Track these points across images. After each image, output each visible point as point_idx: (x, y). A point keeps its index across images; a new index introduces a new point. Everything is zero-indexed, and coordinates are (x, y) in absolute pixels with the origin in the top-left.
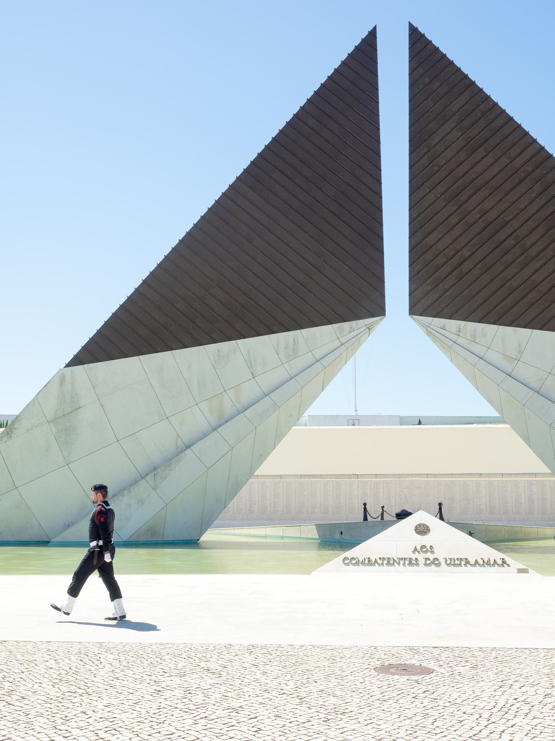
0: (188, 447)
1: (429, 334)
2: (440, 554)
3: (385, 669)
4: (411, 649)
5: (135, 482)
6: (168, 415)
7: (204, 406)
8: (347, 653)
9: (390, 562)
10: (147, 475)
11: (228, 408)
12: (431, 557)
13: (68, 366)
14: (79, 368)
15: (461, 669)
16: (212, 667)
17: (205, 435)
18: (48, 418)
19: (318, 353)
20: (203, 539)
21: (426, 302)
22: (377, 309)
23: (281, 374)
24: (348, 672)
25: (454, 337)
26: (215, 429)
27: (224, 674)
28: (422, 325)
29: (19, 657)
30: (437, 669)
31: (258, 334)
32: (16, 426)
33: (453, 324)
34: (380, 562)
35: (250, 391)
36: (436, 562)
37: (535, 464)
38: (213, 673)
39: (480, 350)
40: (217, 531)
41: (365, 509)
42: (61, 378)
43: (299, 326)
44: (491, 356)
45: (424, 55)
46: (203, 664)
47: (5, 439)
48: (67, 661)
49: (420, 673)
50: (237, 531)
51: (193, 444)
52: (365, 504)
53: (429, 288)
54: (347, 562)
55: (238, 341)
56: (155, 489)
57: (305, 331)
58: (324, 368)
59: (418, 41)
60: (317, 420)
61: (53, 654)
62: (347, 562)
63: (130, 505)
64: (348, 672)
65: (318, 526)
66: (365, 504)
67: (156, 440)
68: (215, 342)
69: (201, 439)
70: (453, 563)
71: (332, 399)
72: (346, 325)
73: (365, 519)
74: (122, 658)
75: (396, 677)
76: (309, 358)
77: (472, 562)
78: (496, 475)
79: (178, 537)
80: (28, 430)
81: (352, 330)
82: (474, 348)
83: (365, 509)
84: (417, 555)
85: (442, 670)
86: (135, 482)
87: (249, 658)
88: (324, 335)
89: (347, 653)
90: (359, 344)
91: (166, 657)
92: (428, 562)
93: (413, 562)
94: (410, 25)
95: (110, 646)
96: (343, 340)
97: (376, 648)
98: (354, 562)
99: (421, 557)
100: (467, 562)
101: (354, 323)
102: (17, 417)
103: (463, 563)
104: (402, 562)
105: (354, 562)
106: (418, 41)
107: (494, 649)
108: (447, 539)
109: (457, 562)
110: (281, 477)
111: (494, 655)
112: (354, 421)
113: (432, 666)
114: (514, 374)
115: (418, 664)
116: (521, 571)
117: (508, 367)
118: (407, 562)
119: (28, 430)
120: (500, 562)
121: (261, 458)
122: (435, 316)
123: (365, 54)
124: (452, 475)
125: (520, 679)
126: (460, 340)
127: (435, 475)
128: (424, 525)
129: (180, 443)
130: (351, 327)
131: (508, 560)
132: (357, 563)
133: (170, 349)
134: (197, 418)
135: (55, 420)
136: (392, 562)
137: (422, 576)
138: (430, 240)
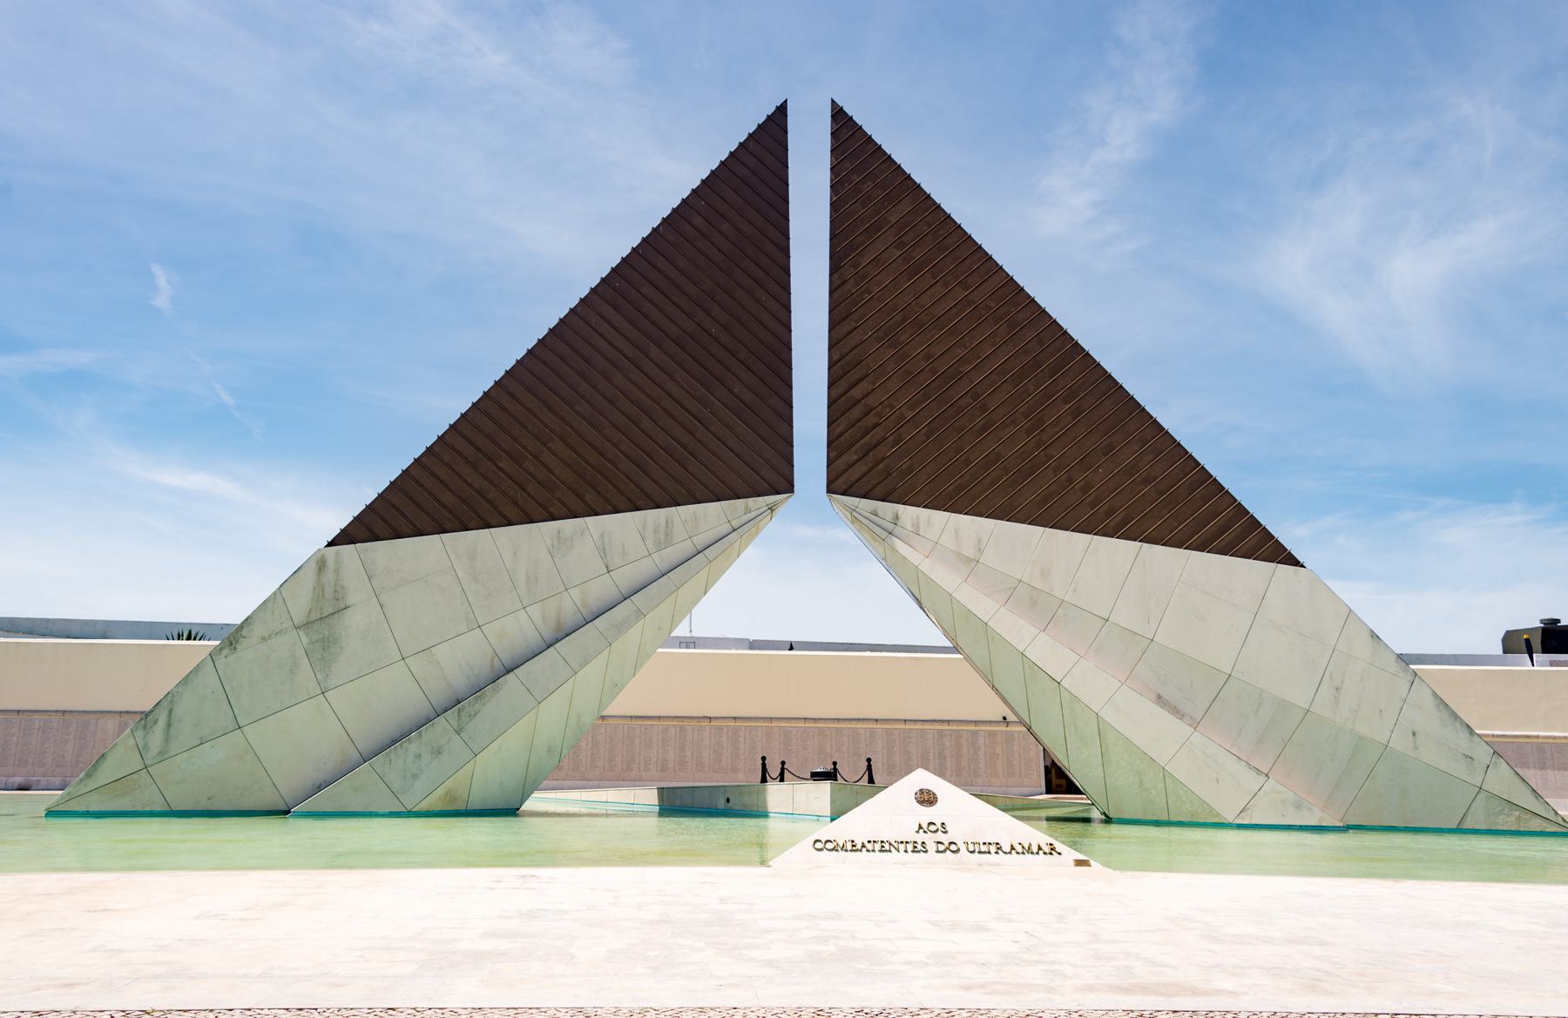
1: (854, 520)
7: (535, 611)
9: (885, 847)
12: (945, 839)
13: (330, 544)
19: (700, 541)
20: (526, 806)
21: (844, 480)
22: (784, 484)
23: (647, 567)
25: (890, 526)
28: (846, 507)
32: (244, 632)
33: (887, 509)
34: (870, 846)
35: (600, 589)
41: (764, 765)
42: (321, 563)
43: (676, 503)
45: (851, 143)
47: (226, 651)
52: (764, 758)
53: (855, 457)
58: (705, 556)
59: (843, 125)
62: (819, 845)
63: (419, 756)
65: (661, 790)
66: (764, 758)
72: (739, 504)
76: (686, 547)
83: (764, 765)
84: (921, 837)
88: (709, 516)
90: (758, 531)
92: (941, 848)
93: (919, 848)
96: (735, 524)
99: (930, 839)
102: (241, 627)
105: (829, 846)
106: (843, 125)
108: (963, 811)
109: (984, 848)
116: (1079, 863)
118: (910, 847)
121: (617, 688)
122: (864, 497)
123: (768, 142)
127: (815, 720)
131: (1059, 846)
132: (854, 849)
135: (306, 625)
136: (887, 846)
137: (933, 869)
138: (856, 392)
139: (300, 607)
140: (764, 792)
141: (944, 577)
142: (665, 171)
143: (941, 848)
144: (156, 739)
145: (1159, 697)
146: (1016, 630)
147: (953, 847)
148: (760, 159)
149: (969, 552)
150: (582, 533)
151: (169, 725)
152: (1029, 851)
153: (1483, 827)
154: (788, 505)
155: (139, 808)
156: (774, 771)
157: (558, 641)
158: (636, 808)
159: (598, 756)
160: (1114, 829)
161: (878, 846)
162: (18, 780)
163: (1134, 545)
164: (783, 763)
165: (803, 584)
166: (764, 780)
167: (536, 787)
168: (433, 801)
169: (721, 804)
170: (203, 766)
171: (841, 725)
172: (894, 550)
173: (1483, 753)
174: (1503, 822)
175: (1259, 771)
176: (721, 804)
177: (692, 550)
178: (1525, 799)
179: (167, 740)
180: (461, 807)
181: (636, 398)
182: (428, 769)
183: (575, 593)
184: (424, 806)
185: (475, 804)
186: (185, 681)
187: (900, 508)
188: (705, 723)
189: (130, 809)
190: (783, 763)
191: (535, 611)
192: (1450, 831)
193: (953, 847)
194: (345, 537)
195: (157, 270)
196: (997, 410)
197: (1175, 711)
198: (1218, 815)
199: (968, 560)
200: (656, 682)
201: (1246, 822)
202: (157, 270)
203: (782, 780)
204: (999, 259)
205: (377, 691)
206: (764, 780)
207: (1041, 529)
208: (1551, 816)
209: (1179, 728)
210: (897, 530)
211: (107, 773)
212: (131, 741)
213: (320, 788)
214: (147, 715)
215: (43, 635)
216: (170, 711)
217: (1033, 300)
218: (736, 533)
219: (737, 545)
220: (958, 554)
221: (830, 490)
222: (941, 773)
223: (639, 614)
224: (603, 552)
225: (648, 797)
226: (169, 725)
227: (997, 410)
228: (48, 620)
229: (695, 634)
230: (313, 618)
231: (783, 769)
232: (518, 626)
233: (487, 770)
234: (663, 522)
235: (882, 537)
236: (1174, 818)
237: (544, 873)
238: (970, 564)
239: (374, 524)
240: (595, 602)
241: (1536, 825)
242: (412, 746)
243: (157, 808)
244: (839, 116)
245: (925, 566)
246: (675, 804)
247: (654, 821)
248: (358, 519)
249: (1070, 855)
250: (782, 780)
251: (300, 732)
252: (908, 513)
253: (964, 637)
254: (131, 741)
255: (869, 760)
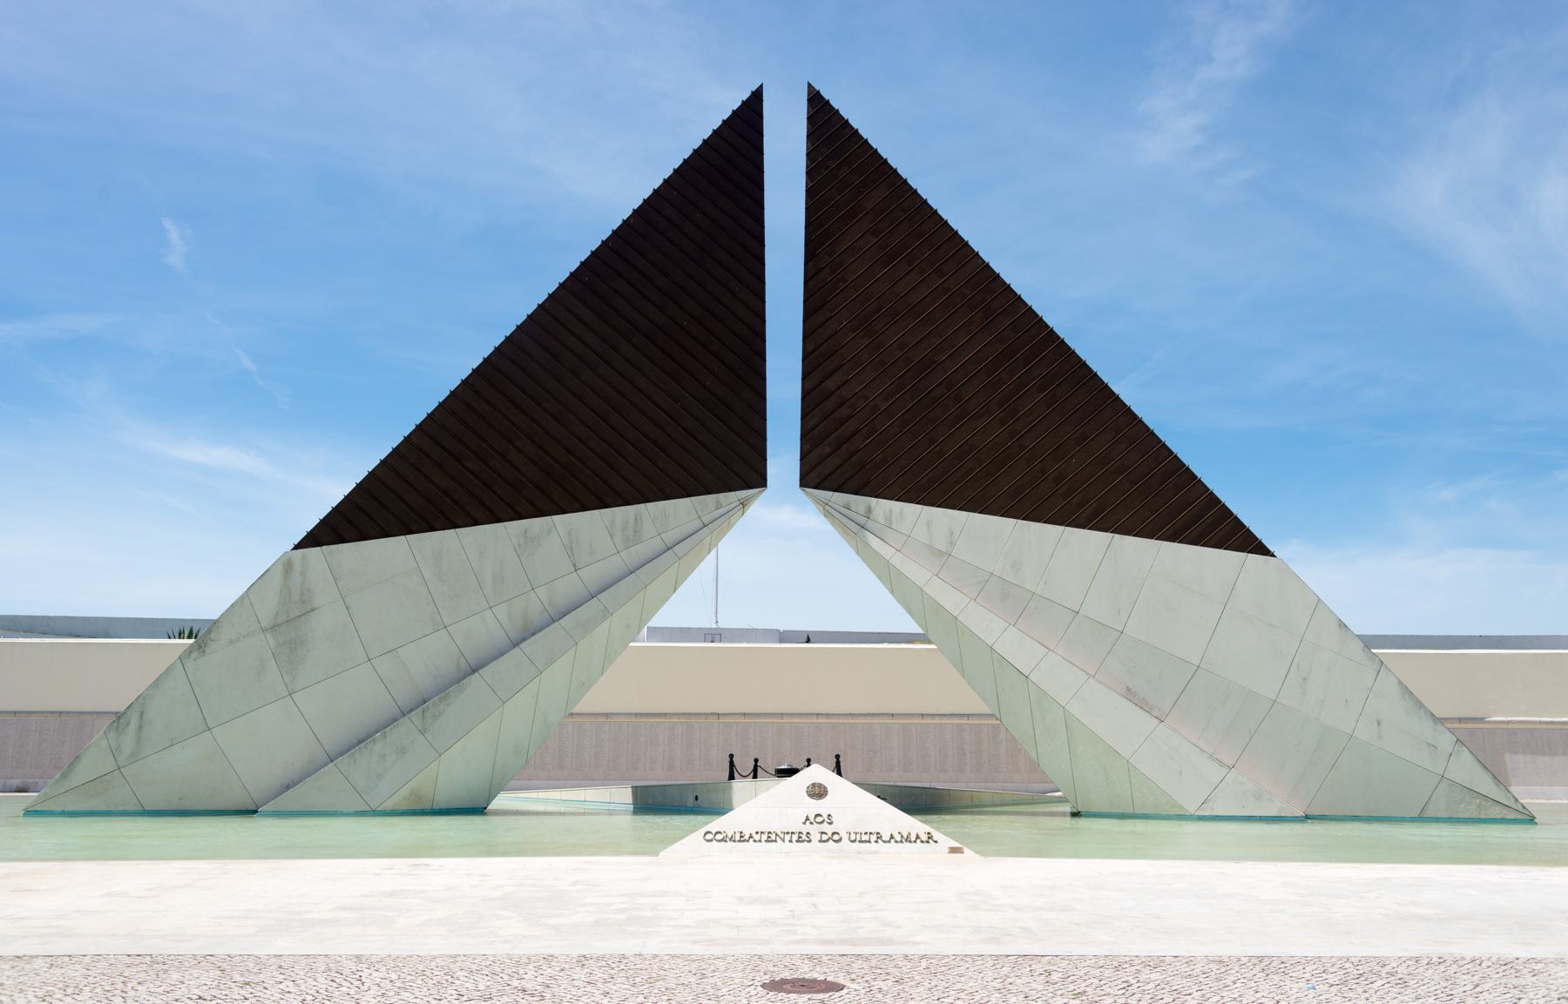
0: (474, 671)
1: (827, 514)
2: (840, 825)
3: (776, 986)
4: (811, 958)
6: (447, 622)
7: (502, 611)
8: (721, 964)
13: (297, 547)
14: (314, 552)
15: (882, 985)
16: (528, 986)
17: (501, 653)
18: (264, 624)
19: (669, 537)
21: (818, 474)
22: (755, 477)
23: (616, 564)
24: (724, 990)
25: (862, 520)
26: (516, 645)
27: (548, 996)
28: (818, 501)
29: (237, 978)
30: (849, 984)
32: (213, 636)
33: (859, 502)
34: (757, 837)
35: (568, 587)
36: (835, 838)
38: (532, 995)
40: (512, 795)
41: (732, 764)
42: (286, 565)
45: (828, 129)
46: (515, 983)
47: (195, 654)
48: (310, 981)
49: (826, 991)
50: (542, 795)
51: (483, 666)
52: (838, 757)
53: (828, 450)
54: (711, 837)
55: (555, 518)
58: (677, 554)
59: (821, 114)
60: (656, 633)
61: (288, 972)
62: (709, 837)
63: (383, 757)
64: (724, 990)
65: (635, 790)
66: (731, 756)
68: (521, 517)
69: (495, 658)
70: (861, 838)
71: (686, 605)
72: (710, 499)
74: (394, 977)
75: (793, 996)
76: (656, 544)
77: (886, 837)
79: (444, 806)
80: (232, 642)
81: (718, 506)
83: (732, 764)
85: (855, 986)
87: (580, 974)
88: (679, 511)
89: (721, 964)
90: (729, 527)
91: (460, 974)
92: (825, 837)
94: (810, 85)
95: (374, 959)
96: (706, 519)
97: (760, 957)
98: (719, 837)
99: (815, 830)
100: (879, 837)
101: (722, 496)
102: (215, 622)
103: (873, 838)
104: (787, 837)
105: (719, 837)
107: (924, 957)
108: (852, 804)
109: (865, 838)
110: (607, 715)
111: (924, 964)
112: (713, 635)
113: (841, 980)
115: (822, 978)
116: (953, 850)
118: (795, 837)
119: (232, 642)
120: (924, 838)
121: (585, 686)
123: (747, 121)
124: (852, 715)
125: (962, 995)
127: (828, 715)
128: (820, 785)
129: (463, 665)
130: (718, 506)
131: (936, 835)
132: (742, 839)
133: (455, 526)
135: (274, 628)
137: (814, 860)
138: (830, 384)
139: (267, 609)
140: (730, 788)
141: (917, 572)
142: (610, 180)
143: (825, 837)
145: (1129, 689)
146: (989, 626)
147: (836, 837)
149: (941, 545)
150: (549, 531)
151: (141, 727)
152: (908, 840)
153: (1445, 815)
154: (767, 494)
155: (113, 808)
156: (744, 765)
157: (524, 640)
158: (612, 807)
159: (565, 757)
160: (1083, 823)
161: (764, 837)
162: (16, 782)
163: (1109, 535)
164: (756, 761)
166: (732, 777)
167: (501, 788)
168: (398, 800)
169: (690, 802)
170: (174, 765)
171: (855, 721)
172: (866, 544)
173: (1446, 740)
174: (1464, 810)
175: (1221, 763)
176: (690, 802)
178: (1486, 785)
179: (139, 740)
180: (428, 806)
181: (606, 392)
182: (404, 770)
183: (542, 592)
184: (388, 805)
185: (441, 803)
186: (156, 683)
187: (873, 501)
188: (713, 720)
189: (104, 808)
190: (756, 761)
191: (502, 611)
192: (1413, 820)
193: (836, 837)
194: (312, 539)
195: (169, 225)
196: (976, 401)
197: (1144, 705)
198: (1181, 807)
199: (940, 553)
201: (1207, 813)
202: (169, 225)
203: (755, 777)
204: (975, 244)
205: (343, 691)
206: (732, 777)
208: (1511, 803)
209: (1146, 721)
210: (870, 524)
211: (82, 773)
212: (104, 743)
213: (288, 788)
214: (119, 716)
215: (44, 634)
216: (142, 714)
217: (1009, 286)
220: (930, 547)
221: (804, 483)
223: (606, 613)
225: (624, 795)
226: (141, 727)
227: (976, 401)
228: (49, 618)
229: (722, 625)
230: (280, 620)
231: (756, 767)
232: (483, 626)
233: (452, 771)
234: (631, 520)
235: (855, 530)
236: (1138, 811)
237: (435, 862)
238: (941, 557)
239: (383, 506)
241: (1496, 812)
242: (377, 747)
243: (130, 808)
245: (897, 560)
246: (650, 802)
247: (629, 819)
248: (324, 522)
249: (945, 842)
250: (755, 777)
251: (266, 738)
252: (882, 506)
253: (935, 626)
254: (104, 743)
255: (838, 757)
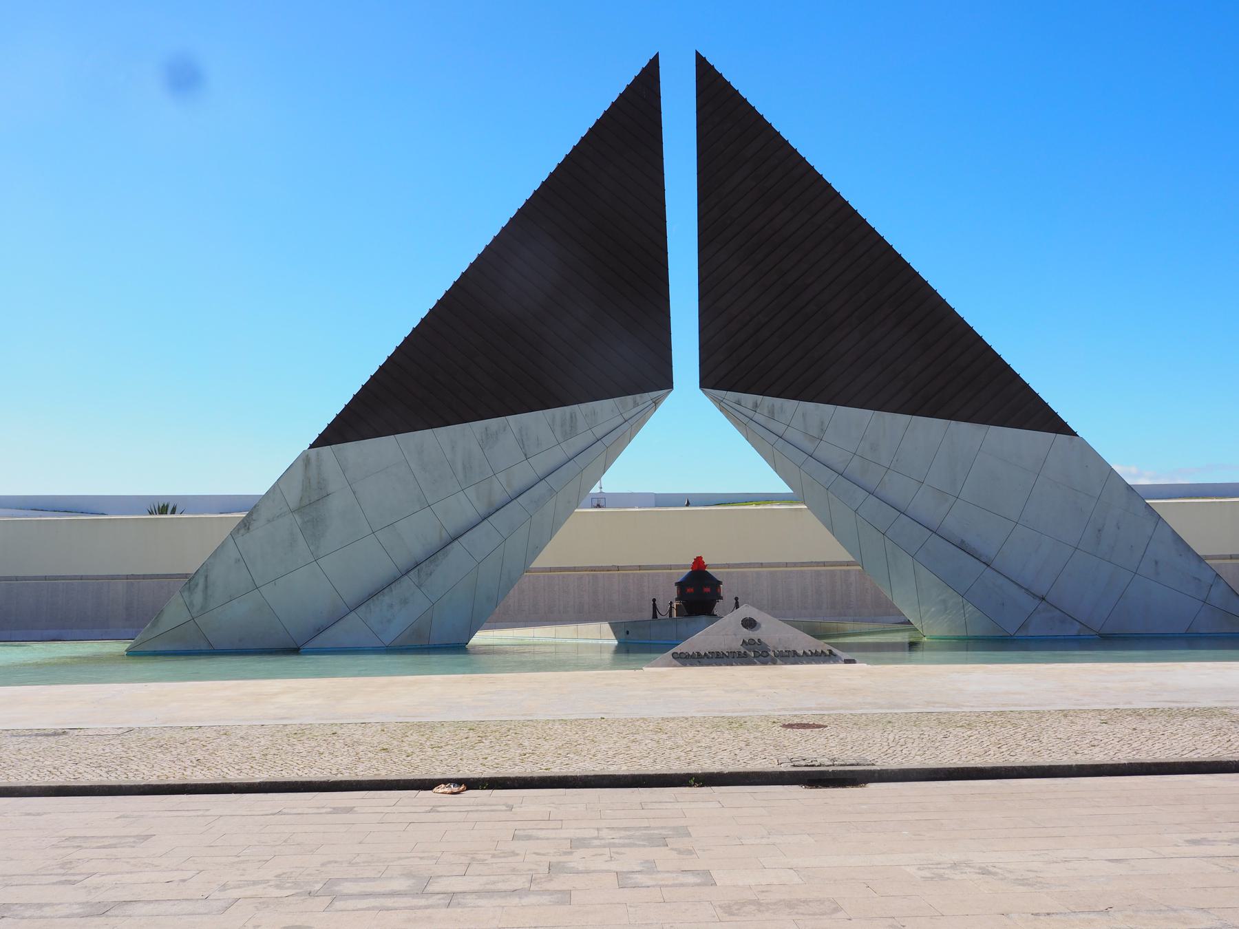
1: (722, 409)
5: (395, 580)
10: (408, 572)
11: (499, 496)
13: (312, 446)
14: (326, 450)
19: (599, 432)
21: (717, 375)
22: (666, 382)
23: (557, 455)
25: (751, 413)
31: (531, 409)
32: (254, 516)
33: (748, 399)
35: (522, 474)
37: (842, 554)
39: (779, 428)
41: (654, 605)
42: (305, 459)
44: (791, 434)
45: (712, 88)
47: (242, 531)
52: (654, 600)
56: (419, 586)
57: (583, 406)
58: (609, 445)
59: (706, 74)
63: (391, 606)
65: (615, 628)
66: (654, 600)
67: (416, 534)
73: (655, 616)
76: (589, 438)
78: (778, 565)
81: (636, 404)
82: (773, 425)
83: (654, 605)
86: (395, 580)
88: (606, 409)
96: (626, 416)
106: (706, 74)
114: (816, 454)
117: (809, 447)
121: (538, 549)
123: (644, 91)
126: (757, 417)
129: (444, 534)
134: (463, 507)
135: (300, 510)
139: (293, 497)
144: (198, 597)
148: (639, 103)
165: (689, 455)
177: (593, 439)
181: (522, 335)
182: (424, 617)
184: (387, 639)
194: (324, 440)
200: (575, 544)
207: (871, 412)
218: (656, 403)
219: (628, 433)
222: (760, 608)
223: (552, 492)
224: (522, 443)
225: (601, 635)
227: (833, 315)
234: (568, 417)
240: (518, 484)
242: (386, 599)
244: (703, 66)
